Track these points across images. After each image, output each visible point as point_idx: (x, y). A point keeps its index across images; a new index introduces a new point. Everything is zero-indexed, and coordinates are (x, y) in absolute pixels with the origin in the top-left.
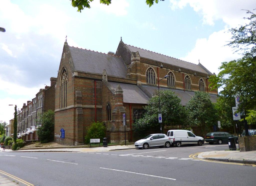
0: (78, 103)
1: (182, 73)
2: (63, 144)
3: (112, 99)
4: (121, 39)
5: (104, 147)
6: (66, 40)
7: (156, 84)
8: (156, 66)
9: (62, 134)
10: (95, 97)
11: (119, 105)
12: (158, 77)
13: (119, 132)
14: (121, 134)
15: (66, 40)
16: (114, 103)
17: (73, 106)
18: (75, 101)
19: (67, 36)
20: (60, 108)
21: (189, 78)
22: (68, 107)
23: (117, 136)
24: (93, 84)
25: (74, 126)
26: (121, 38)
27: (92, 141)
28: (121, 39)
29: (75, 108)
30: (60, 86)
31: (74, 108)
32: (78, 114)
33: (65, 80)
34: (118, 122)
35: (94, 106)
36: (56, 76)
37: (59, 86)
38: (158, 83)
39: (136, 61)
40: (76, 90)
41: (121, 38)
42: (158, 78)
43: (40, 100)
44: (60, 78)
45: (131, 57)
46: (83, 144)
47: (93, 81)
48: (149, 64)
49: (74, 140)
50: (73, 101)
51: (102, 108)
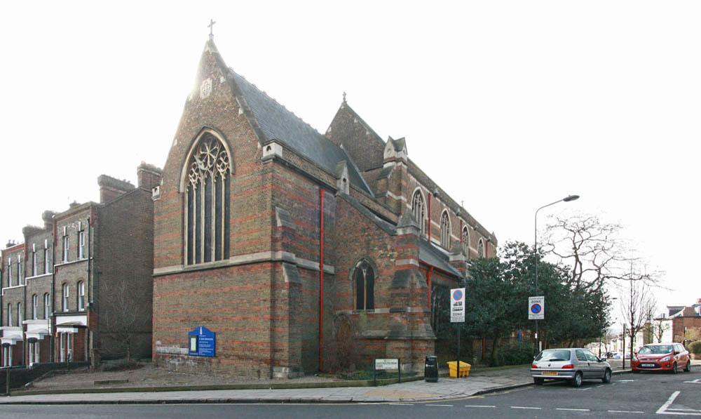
0: (286, 247)
1: (460, 218)
2: (345, 377)
3: (383, 247)
4: (344, 99)
5: (428, 381)
6: (211, 35)
7: (426, 233)
8: (428, 189)
9: (201, 345)
10: (320, 237)
11: (412, 264)
12: (429, 216)
13: (412, 340)
14: (423, 345)
15: (211, 35)
16: (392, 260)
17: (267, 255)
18: (274, 240)
19: (212, 23)
20: (183, 263)
21: (467, 234)
22: (233, 260)
23: (409, 352)
24: (317, 198)
25: (273, 319)
26: (345, 94)
27: (382, 364)
28: (344, 99)
29: (274, 263)
30: (182, 191)
31: (271, 261)
32: (290, 283)
33: (212, 174)
34: (412, 314)
35: (316, 266)
36: (160, 163)
37: (179, 193)
38: (427, 232)
39: (400, 164)
40: (277, 205)
41: (345, 94)
42: (429, 220)
43: (73, 238)
44: (183, 166)
45: (386, 150)
46: (302, 377)
47: (317, 187)
48: (418, 180)
49: (273, 363)
50: (268, 239)
51: (333, 275)
